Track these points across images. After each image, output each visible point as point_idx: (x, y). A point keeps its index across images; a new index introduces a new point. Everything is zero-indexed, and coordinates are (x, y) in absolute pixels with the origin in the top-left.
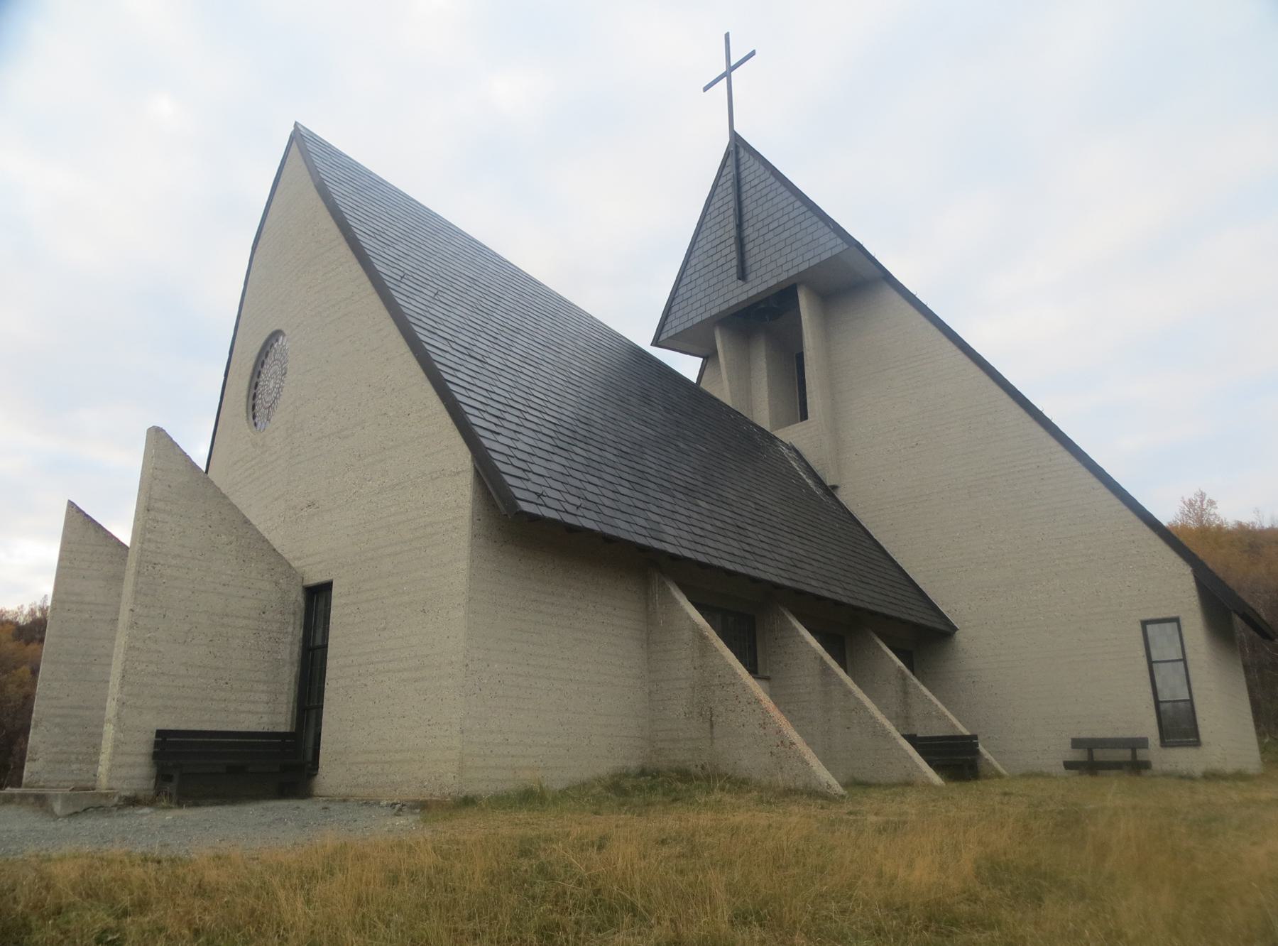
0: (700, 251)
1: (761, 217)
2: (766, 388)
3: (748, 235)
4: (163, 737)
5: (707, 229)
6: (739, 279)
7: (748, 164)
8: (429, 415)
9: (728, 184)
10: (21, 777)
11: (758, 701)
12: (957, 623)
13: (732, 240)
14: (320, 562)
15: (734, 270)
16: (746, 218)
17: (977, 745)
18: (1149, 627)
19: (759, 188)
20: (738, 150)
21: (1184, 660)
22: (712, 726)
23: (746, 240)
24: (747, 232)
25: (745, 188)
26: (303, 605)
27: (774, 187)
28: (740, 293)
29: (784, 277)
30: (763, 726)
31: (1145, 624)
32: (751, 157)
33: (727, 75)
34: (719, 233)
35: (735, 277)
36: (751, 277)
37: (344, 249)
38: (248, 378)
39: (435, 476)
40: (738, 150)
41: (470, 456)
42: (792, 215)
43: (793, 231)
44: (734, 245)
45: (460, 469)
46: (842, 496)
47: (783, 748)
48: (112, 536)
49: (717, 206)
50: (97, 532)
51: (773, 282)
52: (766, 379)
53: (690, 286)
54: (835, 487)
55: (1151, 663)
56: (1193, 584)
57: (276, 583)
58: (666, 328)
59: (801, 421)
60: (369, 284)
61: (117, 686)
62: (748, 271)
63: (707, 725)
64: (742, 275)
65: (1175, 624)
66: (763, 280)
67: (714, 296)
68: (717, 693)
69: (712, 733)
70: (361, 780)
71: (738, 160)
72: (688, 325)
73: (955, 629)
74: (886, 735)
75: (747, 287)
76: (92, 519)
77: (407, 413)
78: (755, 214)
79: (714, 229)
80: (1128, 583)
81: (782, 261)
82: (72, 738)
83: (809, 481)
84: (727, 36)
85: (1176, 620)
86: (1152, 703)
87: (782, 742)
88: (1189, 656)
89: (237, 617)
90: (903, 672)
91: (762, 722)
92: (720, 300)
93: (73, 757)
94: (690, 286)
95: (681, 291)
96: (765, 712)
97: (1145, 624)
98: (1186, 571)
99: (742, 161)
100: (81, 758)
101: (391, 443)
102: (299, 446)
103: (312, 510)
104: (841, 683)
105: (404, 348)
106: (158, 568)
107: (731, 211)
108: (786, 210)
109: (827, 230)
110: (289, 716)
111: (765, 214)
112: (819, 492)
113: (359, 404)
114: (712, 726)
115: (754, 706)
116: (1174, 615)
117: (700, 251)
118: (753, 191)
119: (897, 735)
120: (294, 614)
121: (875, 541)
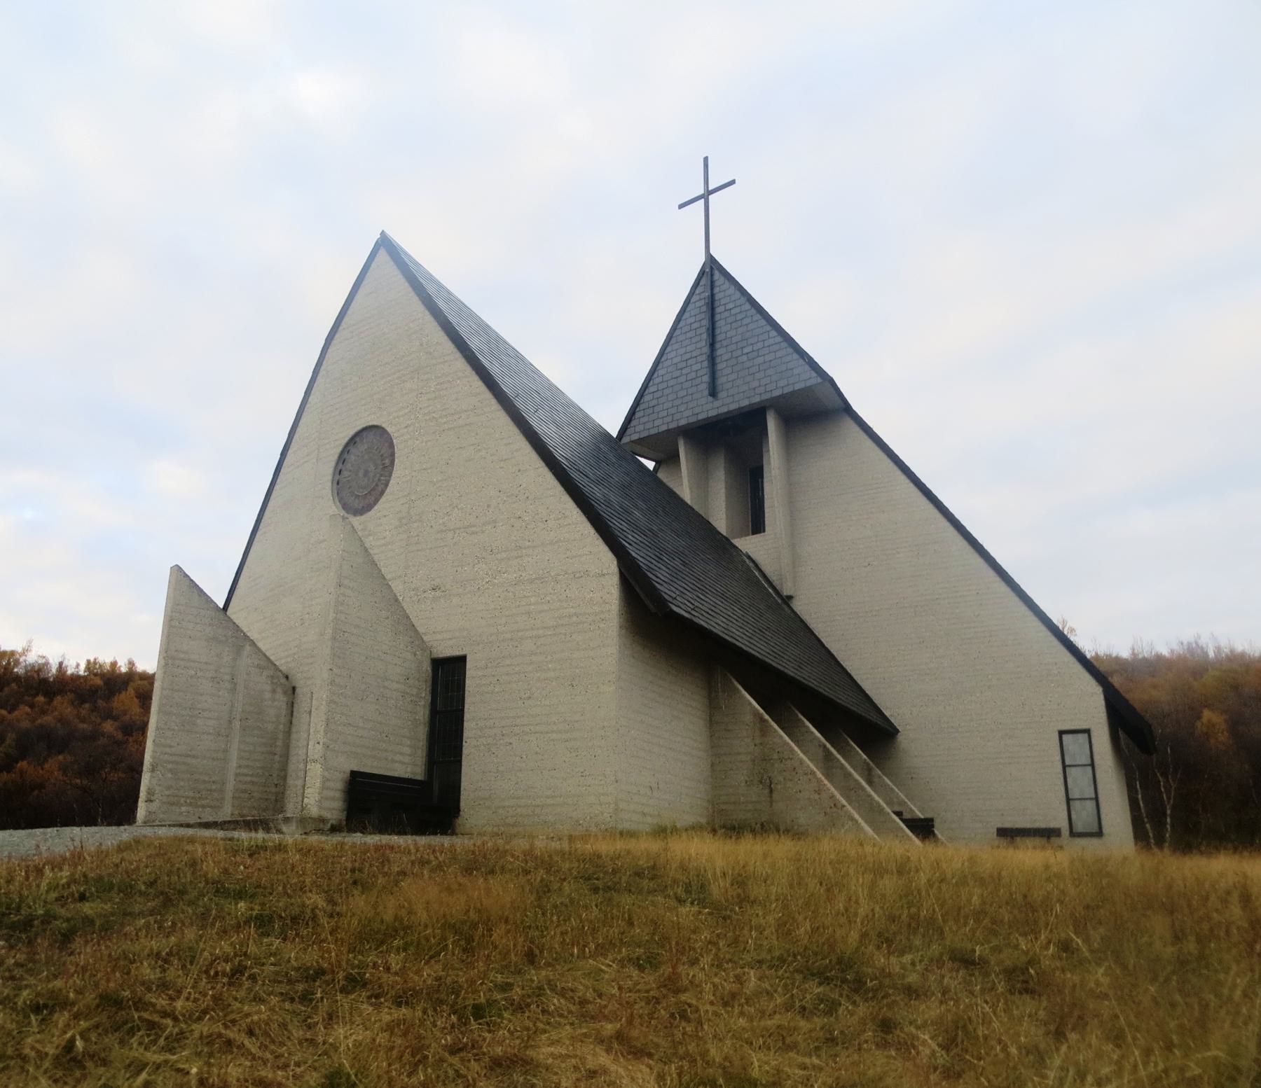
0: (669, 362)
1: (734, 340)
2: (723, 498)
3: (721, 355)
4: (355, 775)
5: (677, 342)
6: (710, 395)
7: (723, 288)
8: (570, 524)
9: (700, 303)
10: (135, 817)
11: (813, 773)
12: (30, 834)
13: (704, 357)
14: (450, 639)
15: (704, 386)
16: (718, 338)
17: (933, 826)
18: (1065, 737)
19: (733, 312)
20: (712, 273)
21: (1092, 765)
22: (771, 791)
23: (718, 360)
24: (719, 352)
25: (718, 310)
26: (431, 675)
27: (749, 313)
28: (707, 409)
29: (756, 399)
30: (818, 792)
31: (1061, 733)
32: (726, 281)
33: (706, 195)
34: (689, 349)
35: (706, 393)
36: (722, 395)
37: (461, 364)
38: (333, 464)
39: (577, 575)
40: (712, 273)
41: (615, 562)
42: (767, 343)
43: (768, 358)
44: (706, 362)
45: (605, 571)
46: (798, 606)
47: (835, 809)
48: (212, 601)
49: (689, 321)
50: (200, 596)
51: (745, 403)
52: (723, 490)
53: (656, 395)
54: (790, 597)
55: (1064, 767)
56: (1103, 703)
57: (415, 655)
58: (629, 432)
59: (753, 534)
60: (494, 401)
61: (322, 731)
62: (719, 388)
63: (767, 791)
64: (713, 393)
65: (1086, 735)
66: (734, 398)
67: (682, 408)
68: (776, 765)
69: (771, 797)
70: (510, 820)
71: (712, 283)
72: (653, 431)
73: (898, 731)
74: (881, 810)
75: (717, 404)
76: (196, 584)
77: (544, 520)
78: (728, 336)
79: (685, 343)
80: (1049, 698)
81: (756, 384)
82: (182, 783)
83: (770, 590)
84: (706, 159)
85: (1087, 731)
86: (1064, 799)
87: (835, 805)
88: (1097, 762)
89: (392, 681)
90: (868, 764)
91: (817, 789)
92: (689, 413)
93: (182, 800)
94: (656, 395)
95: (647, 398)
96: (819, 781)
97: (1061, 733)
98: (1098, 690)
99: (717, 284)
100: (188, 801)
101: (527, 543)
102: (418, 536)
103: (438, 593)
104: (842, 767)
105: (539, 464)
106: (346, 635)
107: (704, 330)
108: (761, 338)
109: (801, 361)
110: (423, 767)
111: (739, 338)
112: (780, 601)
113: (488, 506)
114: (771, 791)
115: (810, 776)
116: (1085, 727)
117: (669, 362)
118: (727, 314)
119: (889, 811)
120: (426, 681)
121: (826, 649)
